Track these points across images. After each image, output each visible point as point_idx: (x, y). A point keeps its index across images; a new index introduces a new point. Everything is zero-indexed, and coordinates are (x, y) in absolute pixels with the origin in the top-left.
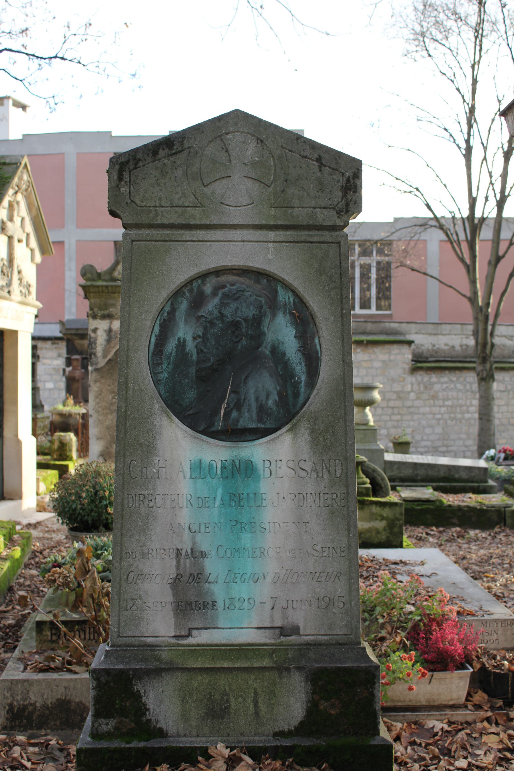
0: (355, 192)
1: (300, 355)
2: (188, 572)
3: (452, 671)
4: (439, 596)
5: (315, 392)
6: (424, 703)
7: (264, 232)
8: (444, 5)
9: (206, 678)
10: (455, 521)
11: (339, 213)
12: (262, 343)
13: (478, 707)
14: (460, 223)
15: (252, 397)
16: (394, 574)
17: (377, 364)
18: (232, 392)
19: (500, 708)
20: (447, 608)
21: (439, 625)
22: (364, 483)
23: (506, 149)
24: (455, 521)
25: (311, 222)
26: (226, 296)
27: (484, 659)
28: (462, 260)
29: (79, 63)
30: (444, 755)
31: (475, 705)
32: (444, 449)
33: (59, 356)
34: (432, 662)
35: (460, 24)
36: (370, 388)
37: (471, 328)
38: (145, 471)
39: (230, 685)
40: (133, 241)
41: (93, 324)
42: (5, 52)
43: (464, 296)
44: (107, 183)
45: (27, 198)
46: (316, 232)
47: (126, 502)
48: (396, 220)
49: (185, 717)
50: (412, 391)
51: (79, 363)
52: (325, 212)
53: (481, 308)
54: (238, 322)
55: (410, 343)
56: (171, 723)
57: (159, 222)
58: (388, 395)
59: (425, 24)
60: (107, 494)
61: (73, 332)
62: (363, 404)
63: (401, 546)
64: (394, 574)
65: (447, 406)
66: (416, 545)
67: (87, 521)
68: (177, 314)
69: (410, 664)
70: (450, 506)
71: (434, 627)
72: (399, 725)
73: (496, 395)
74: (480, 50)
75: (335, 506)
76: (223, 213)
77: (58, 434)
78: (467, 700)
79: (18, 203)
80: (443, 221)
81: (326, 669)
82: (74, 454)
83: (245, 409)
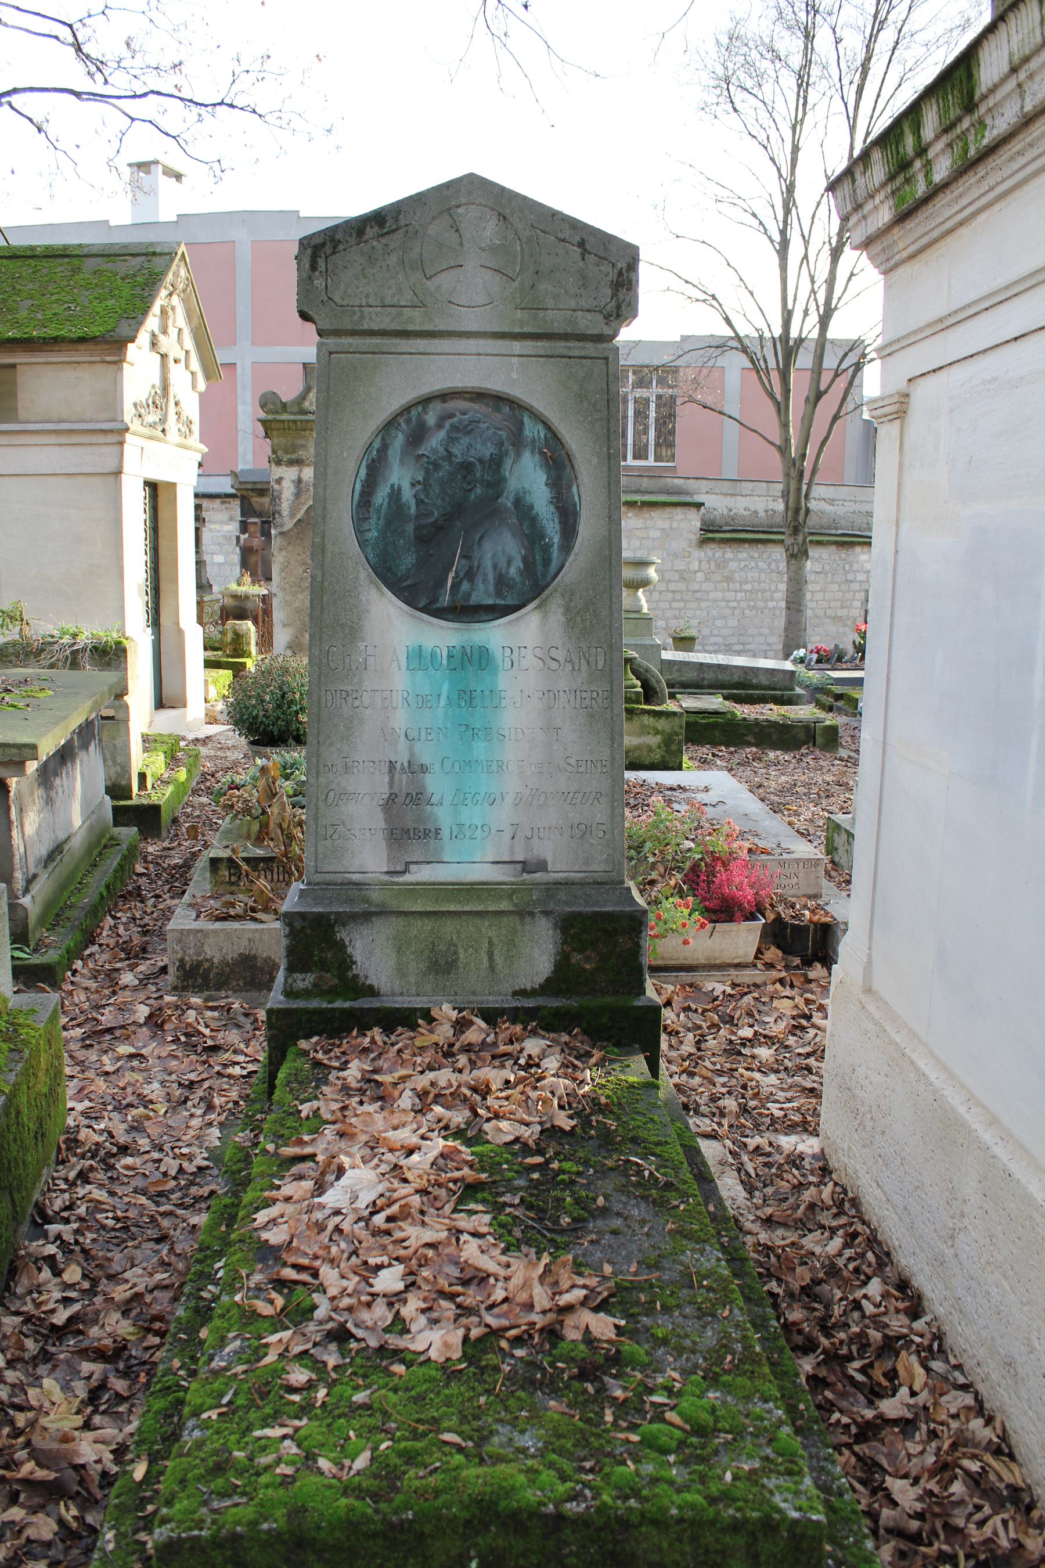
0: (629, 289)
1: (552, 508)
2: (404, 792)
3: (739, 921)
4: (726, 829)
5: (571, 558)
6: (703, 961)
7: (506, 343)
8: (757, 38)
9: (428, 925)
10: (750, 739)
11: (607, 317)
12: (503, 492)
13: (770, 966)
14: (769, 345)
15: (488, 563)
16: (669, 802)
17: (654, 534)
18: (462, 556)
19: (797, 967)
20: (735, 845)
21: (725, 865)
22: (634, 687)
23: (834, 244)
24: (750, 739)
25: (569, 330)
26: (455, 428)
27: (780, 909)
28: (771, 395)
29: (254, 112)
30: (725, 1023)
31: (766, 964)
32: (739, 647)
33: (231, 519)
34: (715, 911)
35: (778, 65)
36: (644, 564)
37: (780, 487)
38: (347, 660)
39: (458, 932)
40: (331, 353)
41: (278, 472)
42: (151, 96)
43: (772, 444)
44: (296, 273)
45: (185, 301)
46: (577, 344)
47: (323, 700)
48: (685, 339)
49: (401, 971)
50: (700, 570)
51: (258, 529)
52: (589, 316)
53: (794, 460)
54: (471, 464)
55: (699, 505)
56: (384, 979)
57: (366, 327)
58: (668, 576)
59: (730, 65)
60: (297, 696)
61: (249, 486)
62: (635, 585)
63: (680, 768)
64: (669, 802)
65: (746, 591)
66: (699, 768)
67: (272, 732)
68: (390, 452)
69: (686, 912)
70: (745, 719)
71: (719, 867)
72: (671, 988)
73: (810, 577)
74: (805, 104)
75: (595, 707)
76: (451, 315)
77: (230, 622)
78: (756, 957)
79: (173, 308)
80: (746, 342)
81: (580, 914)
82: (253, 649)
83: (479, 579)
